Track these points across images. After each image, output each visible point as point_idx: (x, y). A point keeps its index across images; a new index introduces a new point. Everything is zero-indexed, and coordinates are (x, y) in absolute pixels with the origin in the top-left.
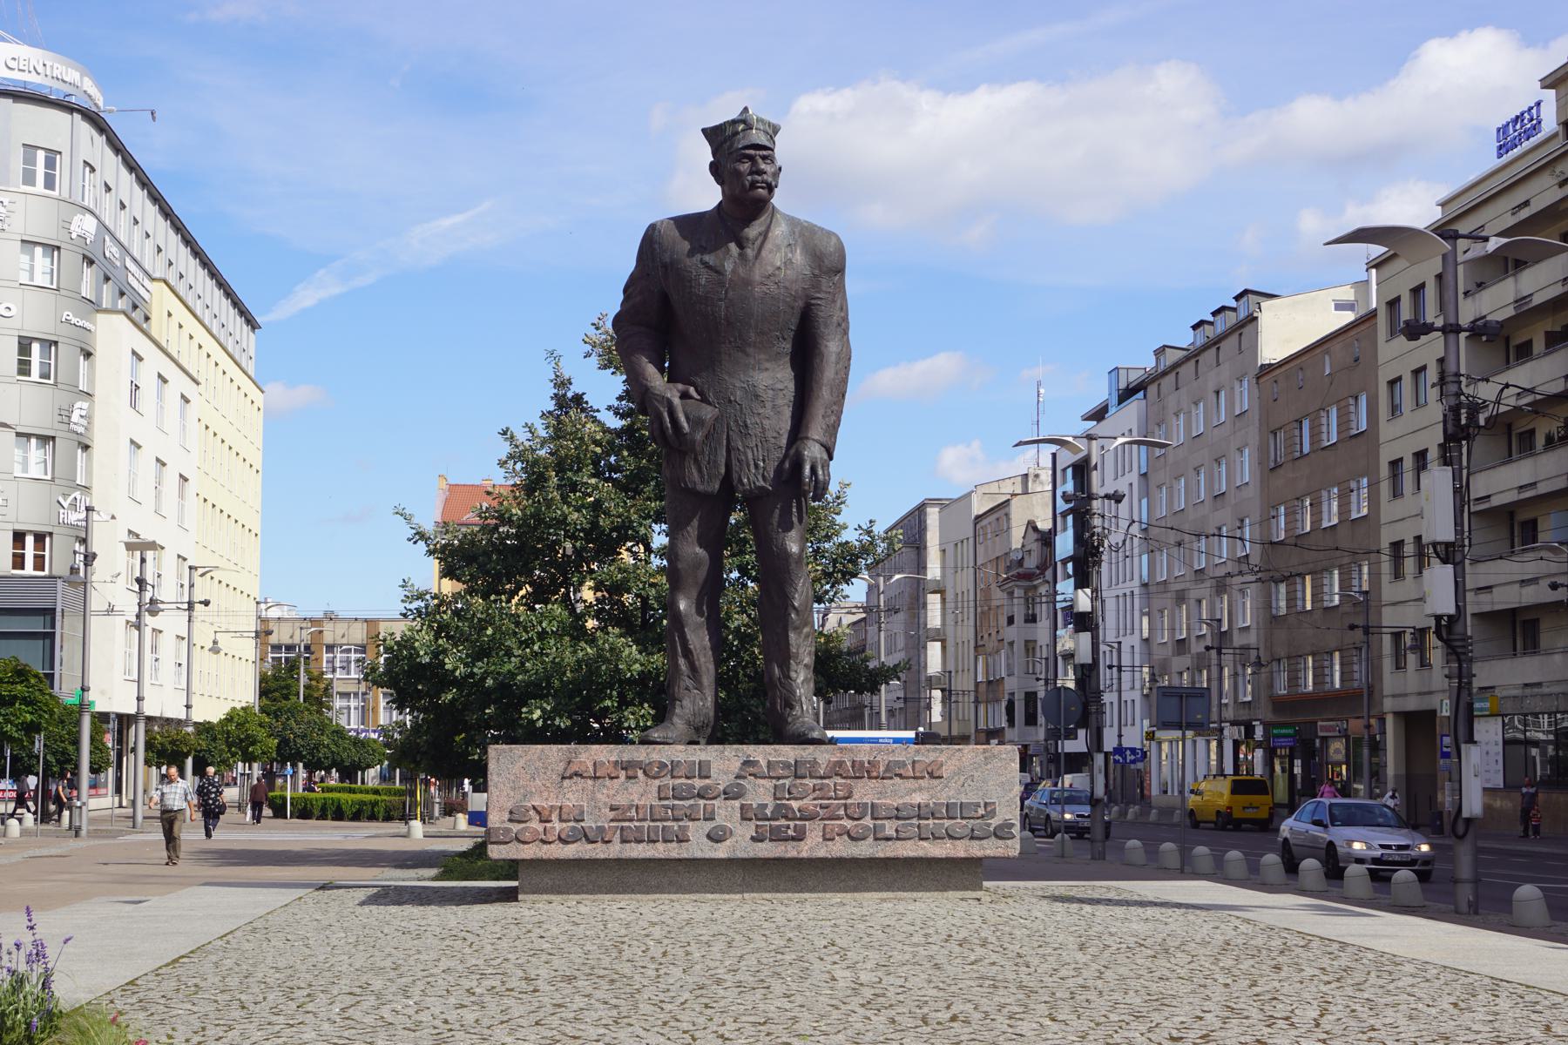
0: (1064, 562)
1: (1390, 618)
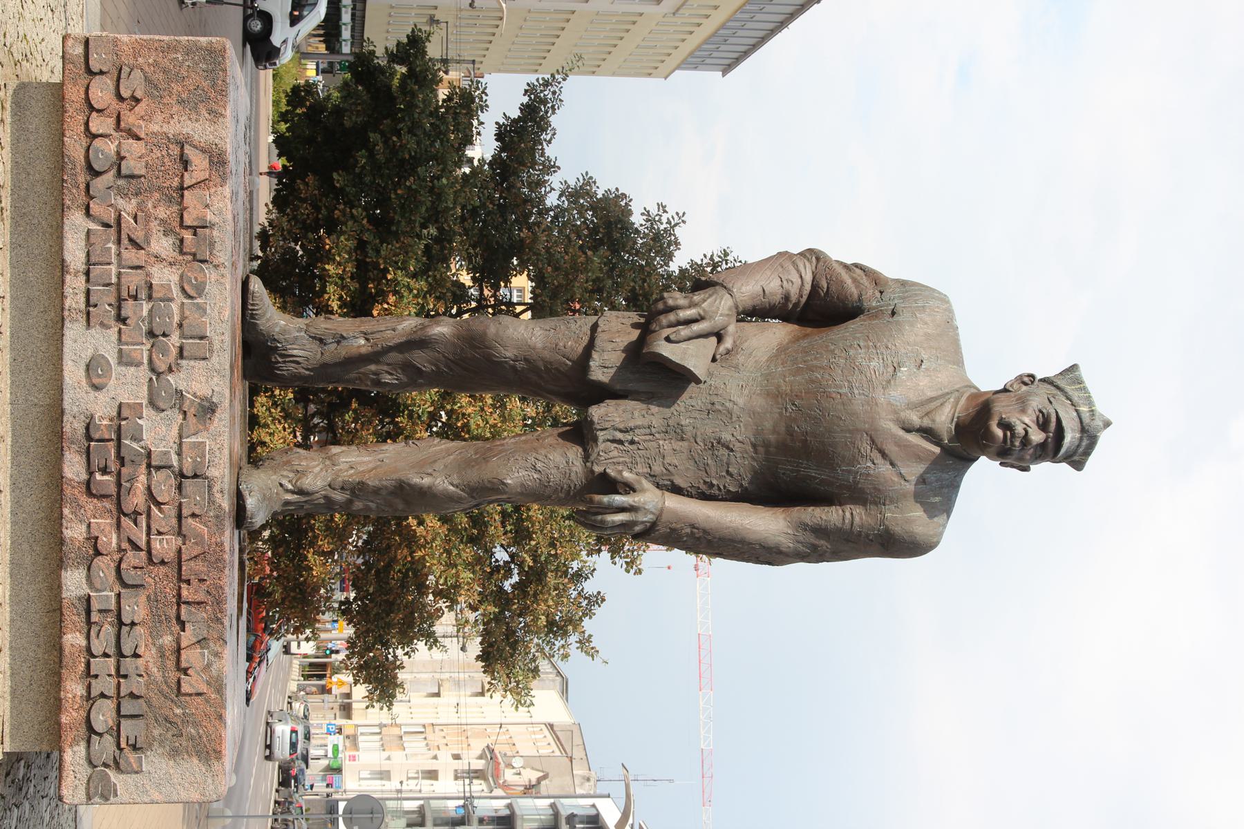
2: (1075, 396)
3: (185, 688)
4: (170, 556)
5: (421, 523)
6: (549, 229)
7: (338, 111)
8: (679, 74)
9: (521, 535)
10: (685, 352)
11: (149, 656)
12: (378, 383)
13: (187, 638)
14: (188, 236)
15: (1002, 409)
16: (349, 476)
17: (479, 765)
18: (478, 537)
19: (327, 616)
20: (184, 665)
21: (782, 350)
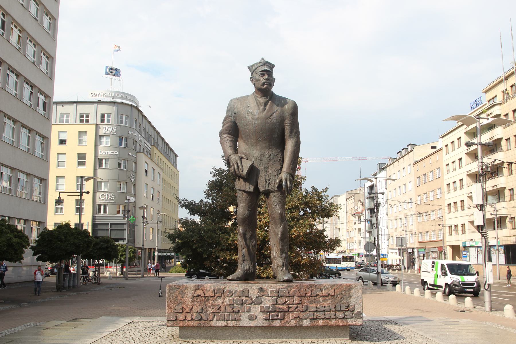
1: (448, 223)
2: (256, 67)
3: (333, 294)
4: (299, 299)
5: (293, 234)
6: (217, 201)
7: (188, 256)
8: (178, 168)
9: (296, 208)
10: (245, 167)
11: (325, 303)
12: (255, 246)
13: (320, 294)
14: (217, 295)
15: (259, 85)
16: (279, 253)
17: (357, 218)
18: (297, 219)
19: (319, 258)
20: (327, 295)
21: (245, 142)
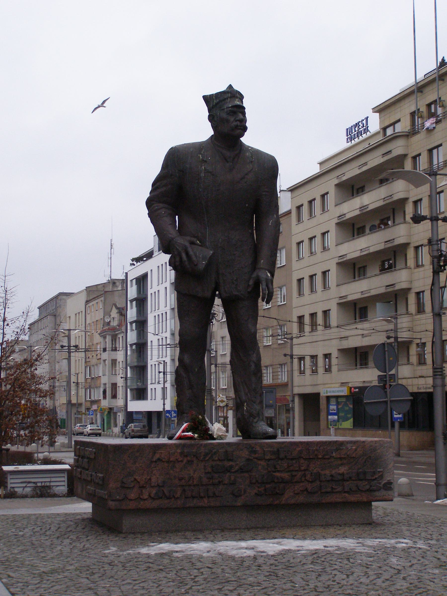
0: (131, 323)
1: (297, 351)
11: (342, 470)
